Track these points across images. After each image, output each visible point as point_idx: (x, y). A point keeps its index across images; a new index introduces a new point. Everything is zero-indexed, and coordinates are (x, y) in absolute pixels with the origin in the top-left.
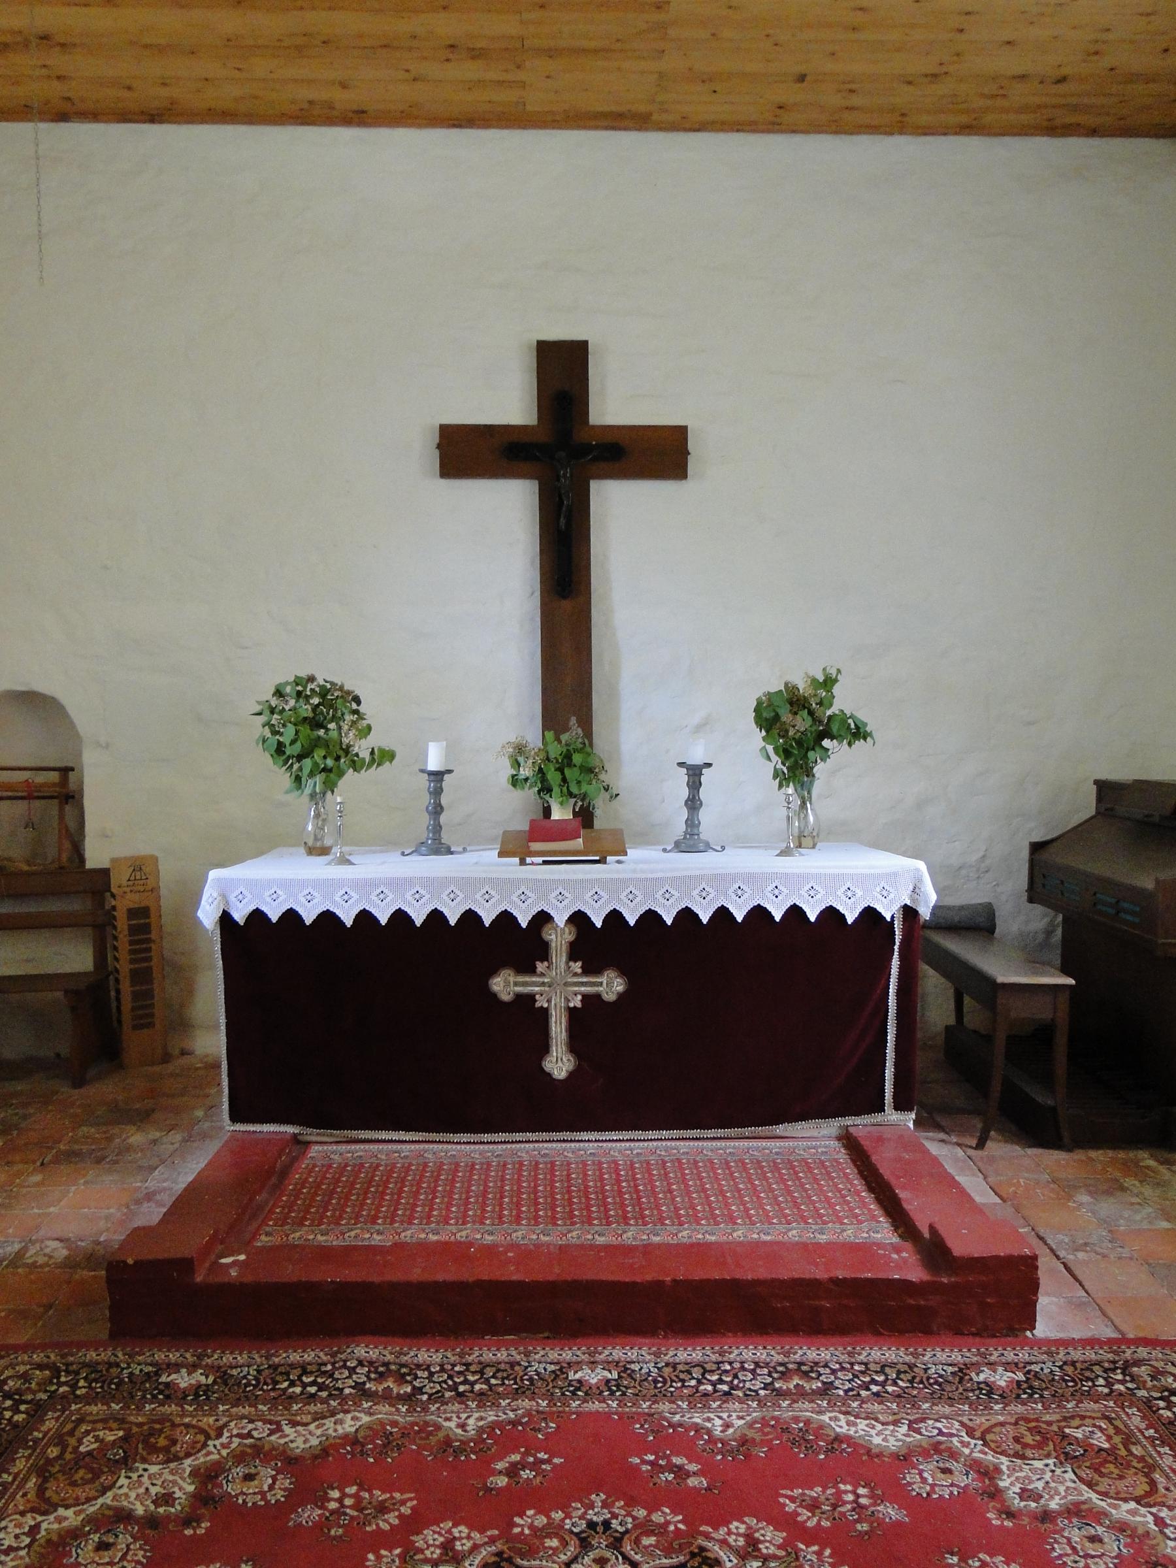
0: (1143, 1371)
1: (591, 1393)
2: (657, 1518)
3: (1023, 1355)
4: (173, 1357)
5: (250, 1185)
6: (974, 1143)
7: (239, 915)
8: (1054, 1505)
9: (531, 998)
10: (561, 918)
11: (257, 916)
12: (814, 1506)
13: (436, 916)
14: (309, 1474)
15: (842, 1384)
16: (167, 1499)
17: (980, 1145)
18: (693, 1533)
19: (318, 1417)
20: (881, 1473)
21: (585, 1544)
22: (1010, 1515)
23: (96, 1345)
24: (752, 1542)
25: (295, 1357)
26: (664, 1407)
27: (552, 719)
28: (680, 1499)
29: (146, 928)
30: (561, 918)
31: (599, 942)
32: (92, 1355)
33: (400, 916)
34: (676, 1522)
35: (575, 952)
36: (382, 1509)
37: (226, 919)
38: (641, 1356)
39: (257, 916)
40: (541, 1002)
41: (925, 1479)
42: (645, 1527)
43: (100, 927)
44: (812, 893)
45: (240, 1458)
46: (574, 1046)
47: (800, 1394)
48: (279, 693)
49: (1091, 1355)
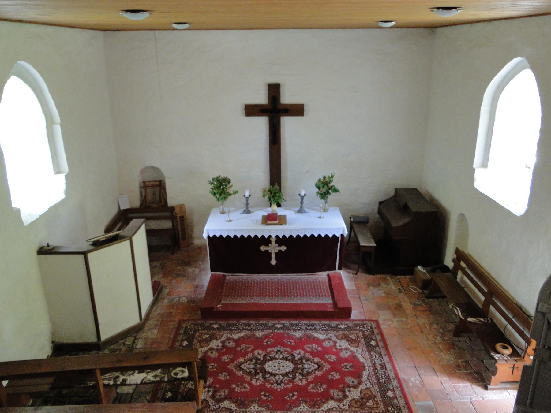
0: (365, 326)
1: (279, 329)
2: (270, 386)
3: (348, 322)
4: (212, 322)
5: (216, 285)
6: (355, 273)
7: (211, 236)
8: (343, 348)
9: (268, 250)
10: (274, 236)
11: (214, 236)
12: (309, 348)
13: (249, 236)
14: (238, 342)
15: (318, 328)
16: (218, 346)
17: (356, 274)
18: (292, 351)
19: (238, 333)
20: (319, 342)
21: (277, 353)
22: (336, 349)
23: (199, 320)
24: (300, 353)
25: (232, 322)
26: (289, 332)
27: (272, 183)
28: (290, 346)
29: (183, 220)
30: (274, 236)
31: (281, 241)
32: (199, 322)
33: (242, 236)
34: (289, 350)
35: (276, 242)
36: (249, 348)
37: (209, 237)
38: (286, 323)
39: (214, 236)
40: (270, 251)
41: (326, 344)
42: (285, 351)
43: (173, 218)
44: (323, 232)
45: (227, 339)
46: (276, 259)
47: (311, 329)
48: (213, 180)
49: (359, 322)
